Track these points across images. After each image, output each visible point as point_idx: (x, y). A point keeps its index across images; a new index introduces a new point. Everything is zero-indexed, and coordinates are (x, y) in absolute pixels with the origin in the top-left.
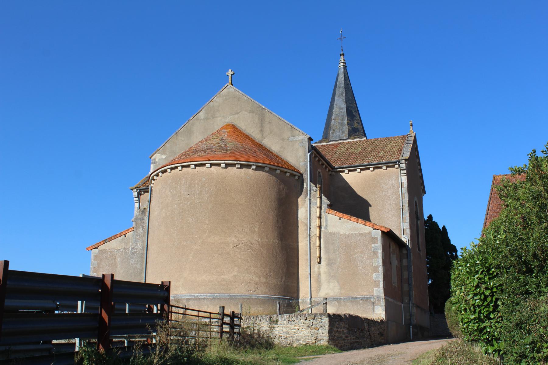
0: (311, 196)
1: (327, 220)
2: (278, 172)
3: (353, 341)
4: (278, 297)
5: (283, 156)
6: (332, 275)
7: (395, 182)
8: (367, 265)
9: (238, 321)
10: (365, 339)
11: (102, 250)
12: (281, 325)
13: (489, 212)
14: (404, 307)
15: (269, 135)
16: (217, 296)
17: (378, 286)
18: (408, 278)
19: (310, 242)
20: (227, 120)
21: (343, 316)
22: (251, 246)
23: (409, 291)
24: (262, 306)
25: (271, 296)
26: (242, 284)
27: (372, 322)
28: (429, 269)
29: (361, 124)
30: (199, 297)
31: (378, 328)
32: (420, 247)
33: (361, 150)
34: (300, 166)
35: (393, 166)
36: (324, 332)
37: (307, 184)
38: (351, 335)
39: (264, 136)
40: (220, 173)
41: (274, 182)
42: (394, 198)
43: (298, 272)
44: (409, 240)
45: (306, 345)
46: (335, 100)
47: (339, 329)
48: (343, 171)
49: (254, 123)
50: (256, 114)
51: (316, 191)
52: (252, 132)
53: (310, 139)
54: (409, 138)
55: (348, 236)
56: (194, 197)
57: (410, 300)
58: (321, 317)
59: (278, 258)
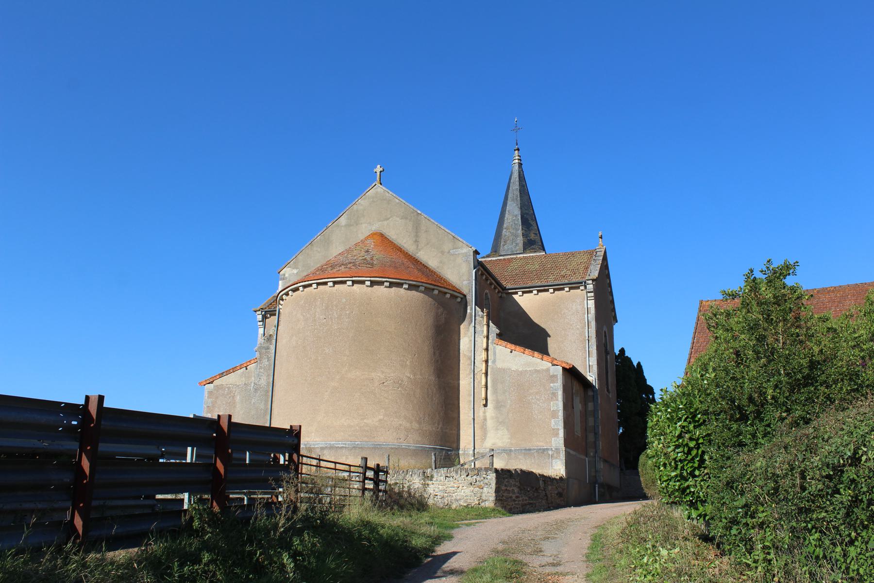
2: (436, 292)
3: (525, 502)
9: (383, 476)
13: (694, 345)
16: (358, 444)
17: (557, 435)
21: (513, 472)
24: (413, 458)
27: (549, 480)
28: (620, 416)
32: (610, 388)
35: (578, 288)
36: (490, 490)
37: (471, 308)
39: (419, 248)
44: (597, 378)
45: (467, 507)
48: (516, 293)
51: (482, 317)
52: (405, 243)
53: (476, 253)
55: (521, 373)
56: (332, 322)
57: (596, 452)
59: (434, 399)
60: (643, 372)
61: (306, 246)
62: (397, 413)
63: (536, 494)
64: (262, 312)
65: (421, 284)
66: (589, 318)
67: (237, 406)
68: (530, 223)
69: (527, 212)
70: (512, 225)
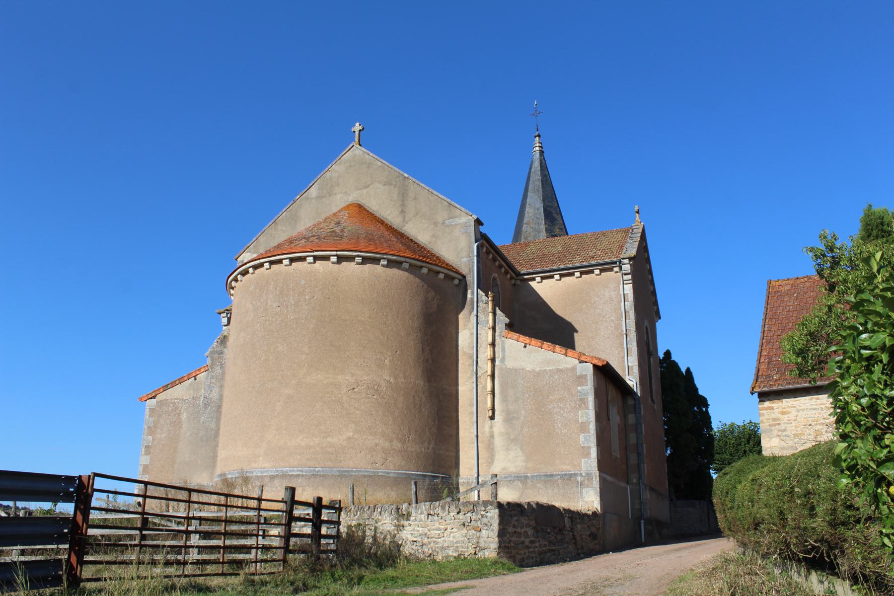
0: (479, 311)
1: (504, 349)
2: (425, 271)
3: (544, 549)
4: (423, 475)
5: (435, 250)
6: (512, 437)
7: (613, 294)
8: (569, 420)
9: (335, 515)
10: (566, 545)
11: (161, 401)
12: (416, 521)
13: (765, 335)
14: (630, 489)
15: (414, 218)
16: (319, 471)
17: (588, 455)
18: (637, 444)
19: (477, 385)
20: (351, 198)
21: (526, 507)
22: (377, 391)
23: (638, 465)
24: (394, 488)
25: (410, 472)
26: (361, 452)
27: (578, 516)
28: (667, 433)
29: (564, 230)
30: (290, 474)
31: (588, 526)
32: (654, 398)
33: (561, 249)
34: (463, 265)
35: (611, 269)
36: (491, 534)
37: (473, 292)
38: (540, 539)
39: (406, 219)
40: (329, 271)
41: (417, 287)
42: (612, 318)
43: (458, 433)
44: (638, 383)
45: (457, 558)
46: (528, 197)
47: (519, 529)
48: (533, 279)
49: (391, 200)
50: (395, 186)
51: (487, 303)
52: (389, 215)
53: (478, 222)
54: (635, 230)
55: (539, 374)
56: (288, 311)
57: (640, 478)
58: (485, 507)
59: (423, 410)
60: (693, 380)
61: (268, 225)
62: (372, 429)
63: (559, 537)
64: (227, 314)
65: (403, 259)
66: (626, 307)
67: (183, 426)
68: (554, 217)
69: (550, 204)
70: (533, 220)
